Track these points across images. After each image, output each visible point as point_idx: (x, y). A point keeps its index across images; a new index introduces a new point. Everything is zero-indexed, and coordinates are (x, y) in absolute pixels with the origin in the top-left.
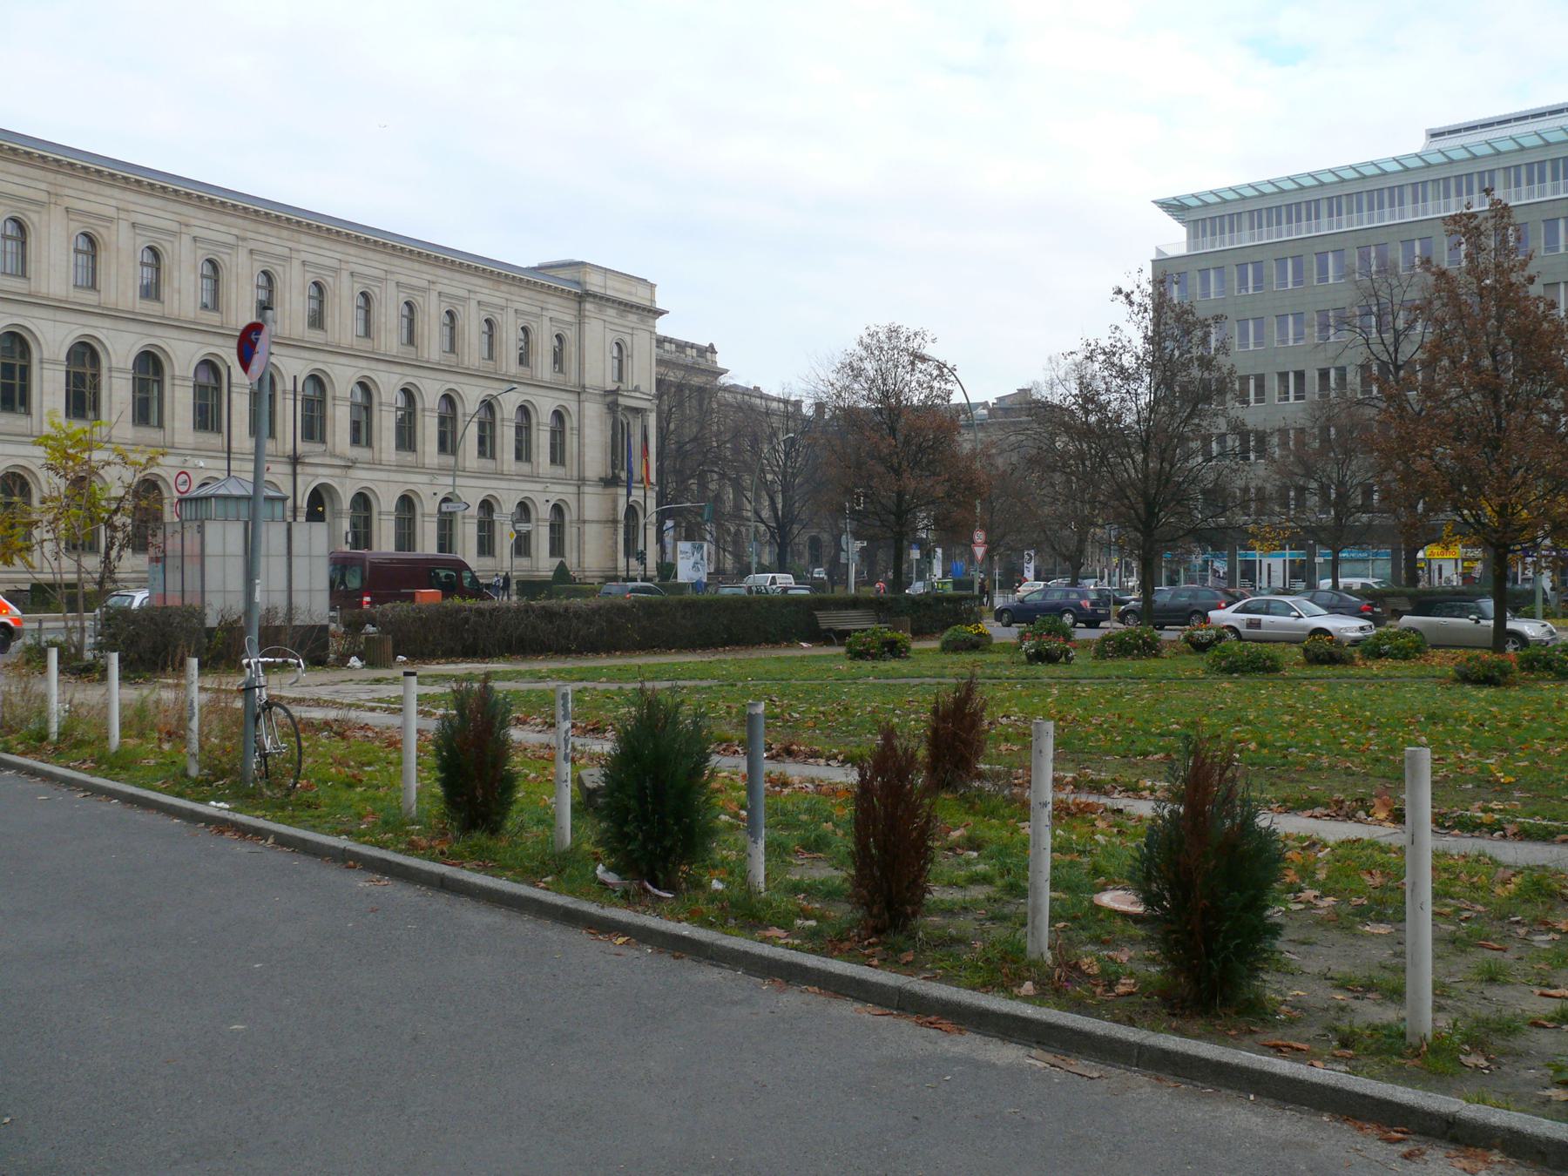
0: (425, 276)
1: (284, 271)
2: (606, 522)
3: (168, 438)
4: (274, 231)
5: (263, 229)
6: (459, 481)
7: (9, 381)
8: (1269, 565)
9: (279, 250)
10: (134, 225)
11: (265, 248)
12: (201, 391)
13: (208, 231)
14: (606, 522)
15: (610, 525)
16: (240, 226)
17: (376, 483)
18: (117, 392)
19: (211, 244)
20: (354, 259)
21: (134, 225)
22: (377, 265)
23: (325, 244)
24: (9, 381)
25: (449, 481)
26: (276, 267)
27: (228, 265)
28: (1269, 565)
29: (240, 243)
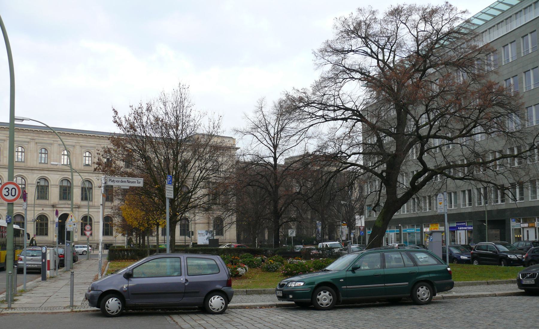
0: (29, 137)
1: (51, 148)
2: (207, 223)
3: (93, 204)
4: (46, 136)
5: (41, 136)
6: (90, 210)
7: (486, 213)
8: (460, 233)
9: (48, 142)
10: (81, 146)
11: (40, 141)
12: (84, 190)
13: (18, 138)
14: (207, 223)
15: (207, 224)
16: (31, 136)
17: (92, 212)
18: (77, 193)
19: (20, 142)
20: (82, 142)
21: (81, 146)
22: (93, 143)
23: (69, 138)
24: (486, 213)
25: (87, 210)
26: (47, 147)
27: (27, 148)
28: (460, 233)
29: (31, 141)
